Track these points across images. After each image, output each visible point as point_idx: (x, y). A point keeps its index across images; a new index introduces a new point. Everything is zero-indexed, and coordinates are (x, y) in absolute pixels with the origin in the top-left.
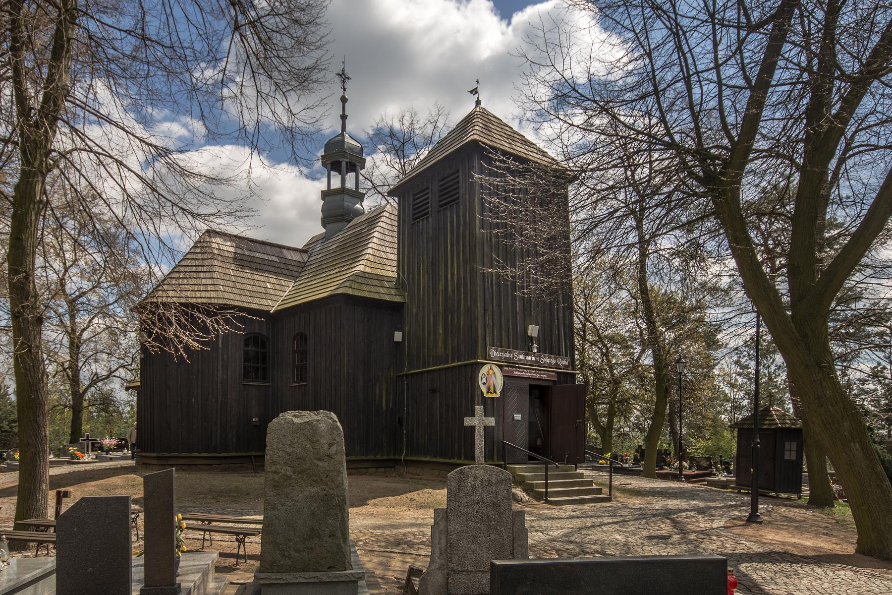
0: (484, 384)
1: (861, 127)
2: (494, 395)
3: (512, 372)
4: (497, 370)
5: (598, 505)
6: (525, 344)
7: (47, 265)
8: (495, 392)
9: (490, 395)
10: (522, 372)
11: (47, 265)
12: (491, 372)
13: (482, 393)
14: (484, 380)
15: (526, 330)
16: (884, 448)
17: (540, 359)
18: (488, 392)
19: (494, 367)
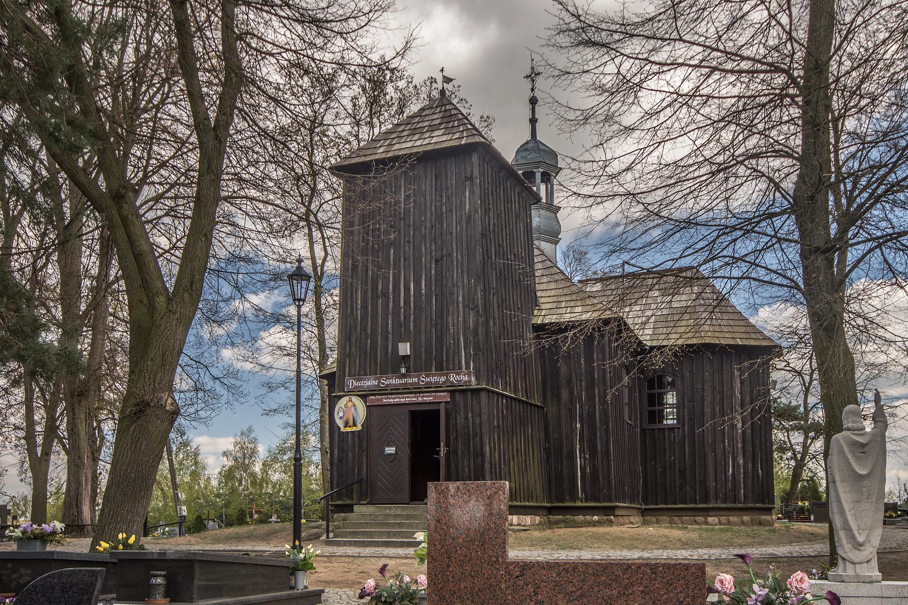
0: (341, 418)
1: (807, 384)
2: (354, 429)
3: (382, 400)
4: (357, 401)
5: (398, 561)
6: (394, 364)
7: (788, 368)
8: (355, 425)
9: (348, 429)
10: (395, 398)
11: (788, 368)
12: (350, 404)
13: (339, 428)
14: (341, 414)
15: (396, 349)
16: (415, 161)
17: (419, 379)
18: (345, 427)
19: (354, 399)
